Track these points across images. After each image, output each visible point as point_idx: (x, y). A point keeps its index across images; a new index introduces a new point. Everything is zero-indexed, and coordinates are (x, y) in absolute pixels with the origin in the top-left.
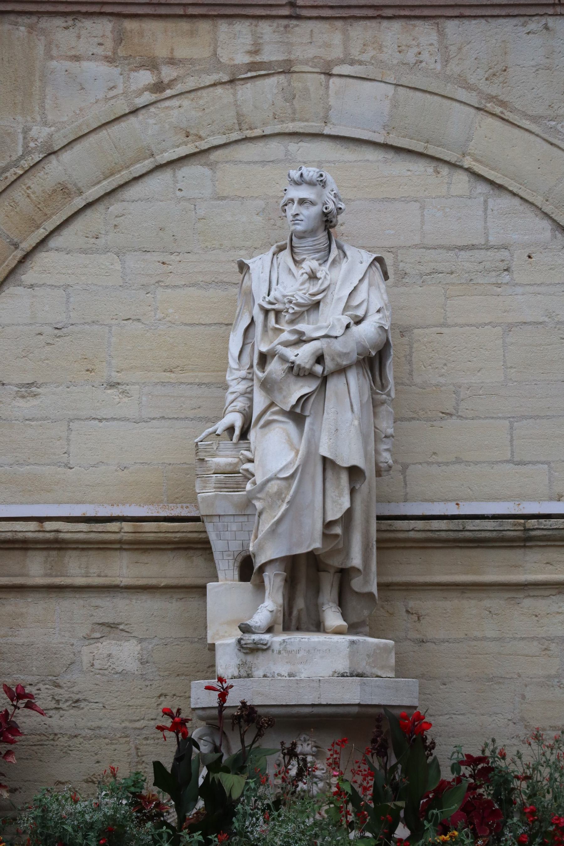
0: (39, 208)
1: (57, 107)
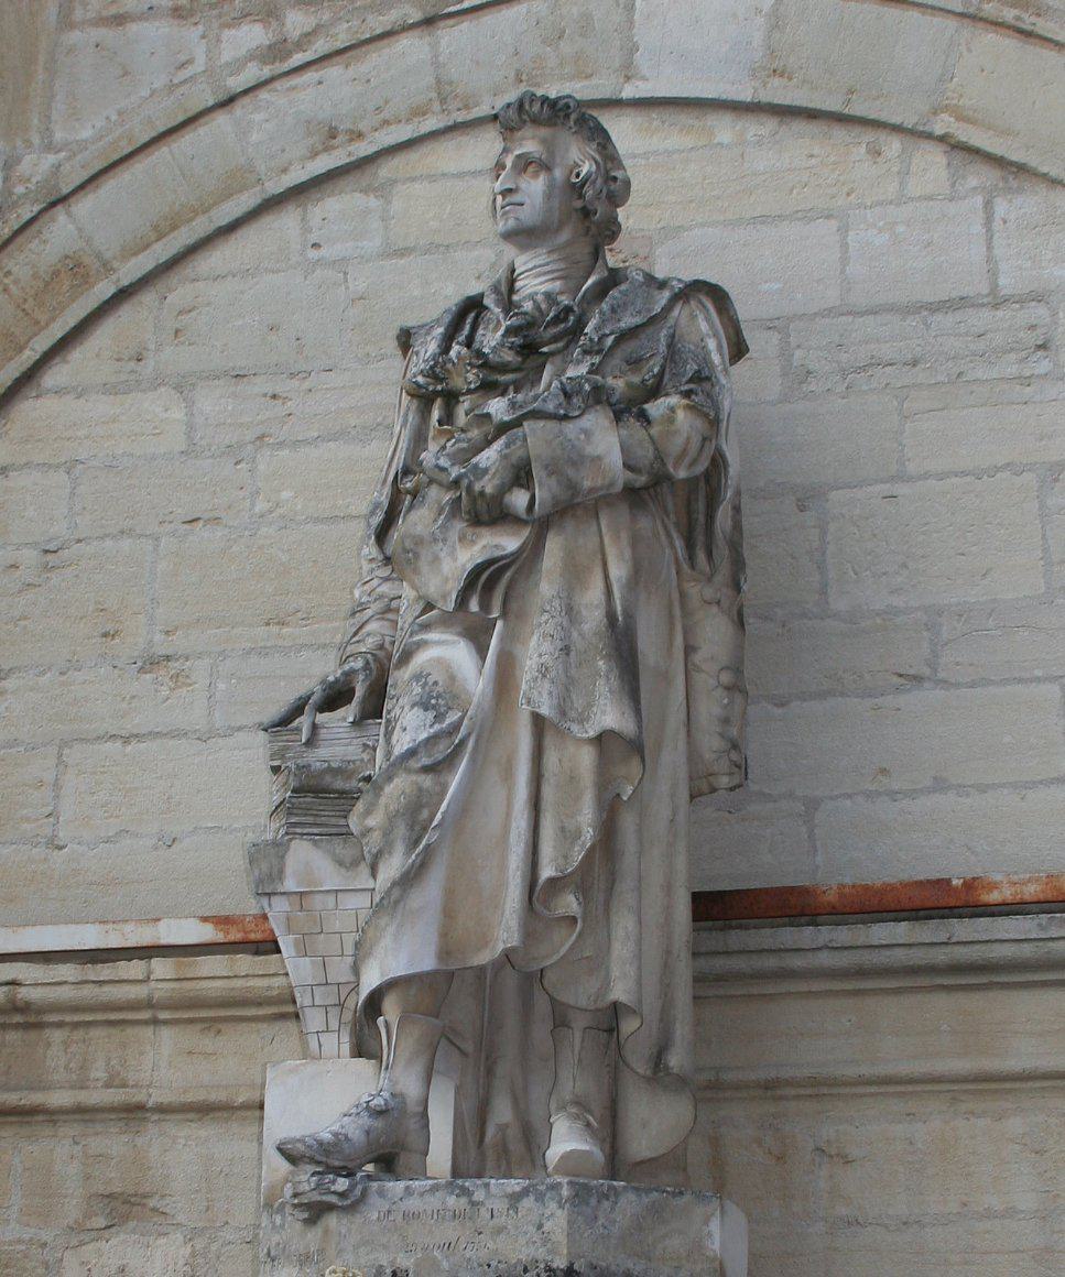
0: (24, 310)
1: (74, 114)
